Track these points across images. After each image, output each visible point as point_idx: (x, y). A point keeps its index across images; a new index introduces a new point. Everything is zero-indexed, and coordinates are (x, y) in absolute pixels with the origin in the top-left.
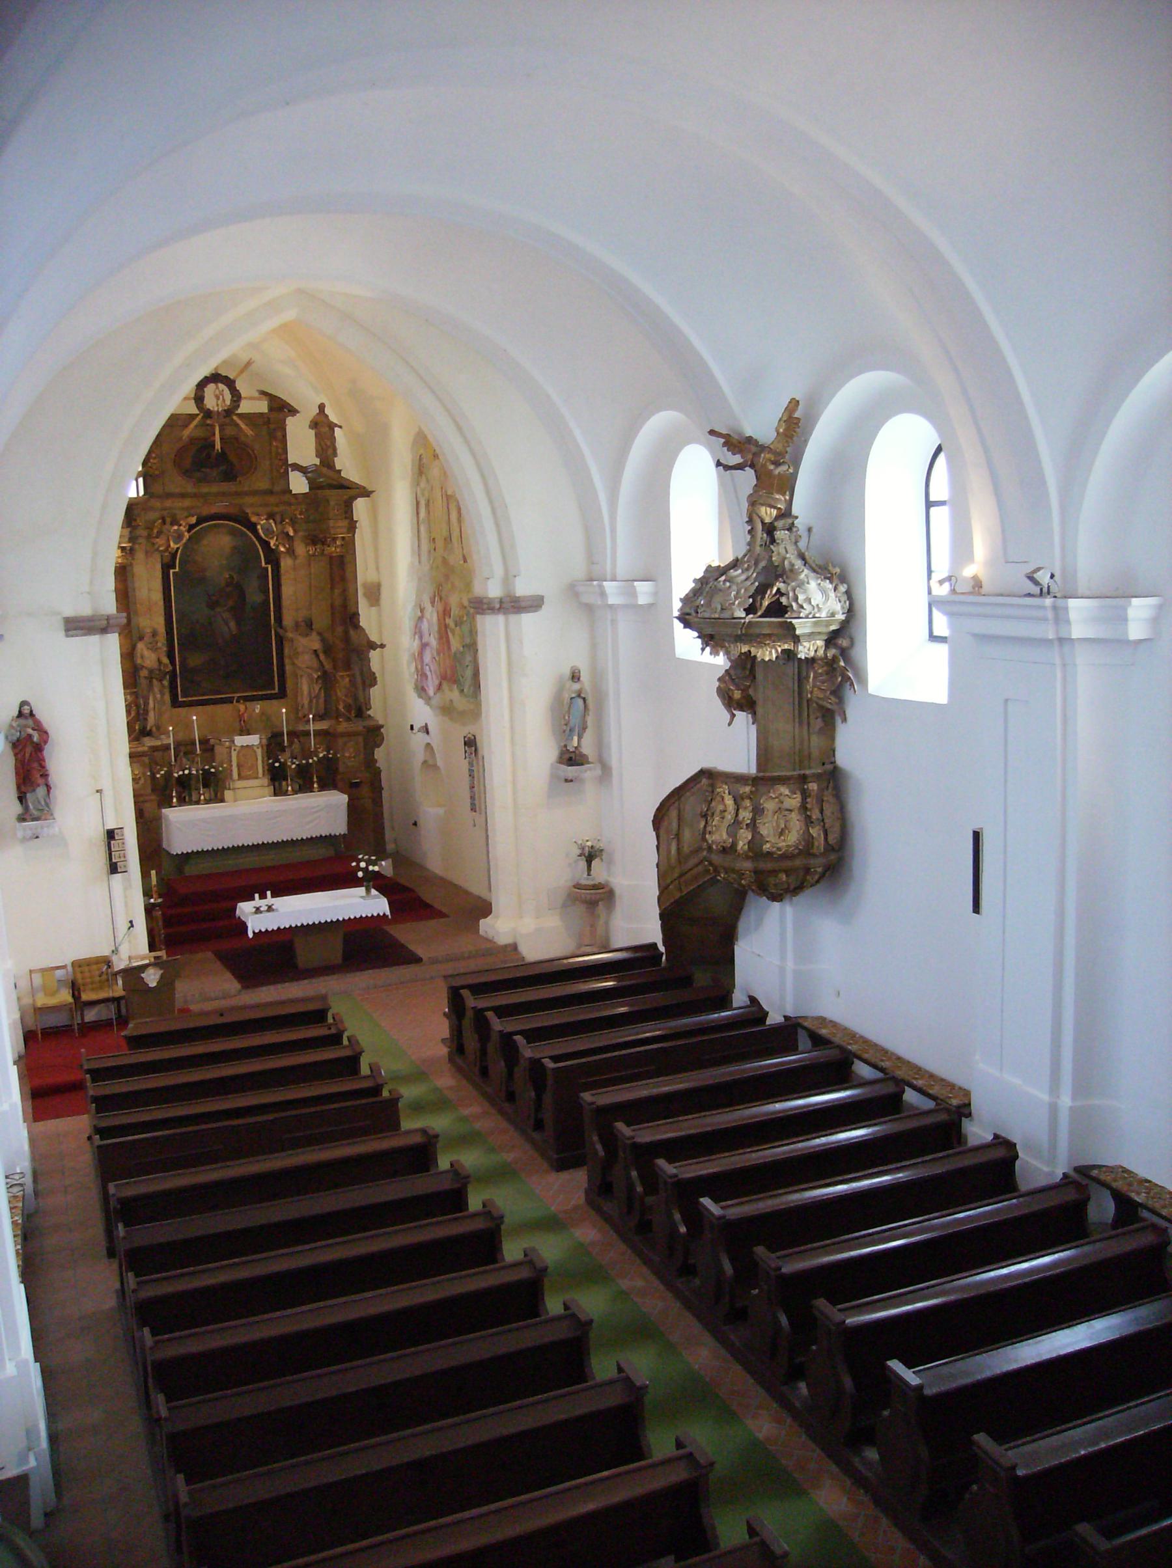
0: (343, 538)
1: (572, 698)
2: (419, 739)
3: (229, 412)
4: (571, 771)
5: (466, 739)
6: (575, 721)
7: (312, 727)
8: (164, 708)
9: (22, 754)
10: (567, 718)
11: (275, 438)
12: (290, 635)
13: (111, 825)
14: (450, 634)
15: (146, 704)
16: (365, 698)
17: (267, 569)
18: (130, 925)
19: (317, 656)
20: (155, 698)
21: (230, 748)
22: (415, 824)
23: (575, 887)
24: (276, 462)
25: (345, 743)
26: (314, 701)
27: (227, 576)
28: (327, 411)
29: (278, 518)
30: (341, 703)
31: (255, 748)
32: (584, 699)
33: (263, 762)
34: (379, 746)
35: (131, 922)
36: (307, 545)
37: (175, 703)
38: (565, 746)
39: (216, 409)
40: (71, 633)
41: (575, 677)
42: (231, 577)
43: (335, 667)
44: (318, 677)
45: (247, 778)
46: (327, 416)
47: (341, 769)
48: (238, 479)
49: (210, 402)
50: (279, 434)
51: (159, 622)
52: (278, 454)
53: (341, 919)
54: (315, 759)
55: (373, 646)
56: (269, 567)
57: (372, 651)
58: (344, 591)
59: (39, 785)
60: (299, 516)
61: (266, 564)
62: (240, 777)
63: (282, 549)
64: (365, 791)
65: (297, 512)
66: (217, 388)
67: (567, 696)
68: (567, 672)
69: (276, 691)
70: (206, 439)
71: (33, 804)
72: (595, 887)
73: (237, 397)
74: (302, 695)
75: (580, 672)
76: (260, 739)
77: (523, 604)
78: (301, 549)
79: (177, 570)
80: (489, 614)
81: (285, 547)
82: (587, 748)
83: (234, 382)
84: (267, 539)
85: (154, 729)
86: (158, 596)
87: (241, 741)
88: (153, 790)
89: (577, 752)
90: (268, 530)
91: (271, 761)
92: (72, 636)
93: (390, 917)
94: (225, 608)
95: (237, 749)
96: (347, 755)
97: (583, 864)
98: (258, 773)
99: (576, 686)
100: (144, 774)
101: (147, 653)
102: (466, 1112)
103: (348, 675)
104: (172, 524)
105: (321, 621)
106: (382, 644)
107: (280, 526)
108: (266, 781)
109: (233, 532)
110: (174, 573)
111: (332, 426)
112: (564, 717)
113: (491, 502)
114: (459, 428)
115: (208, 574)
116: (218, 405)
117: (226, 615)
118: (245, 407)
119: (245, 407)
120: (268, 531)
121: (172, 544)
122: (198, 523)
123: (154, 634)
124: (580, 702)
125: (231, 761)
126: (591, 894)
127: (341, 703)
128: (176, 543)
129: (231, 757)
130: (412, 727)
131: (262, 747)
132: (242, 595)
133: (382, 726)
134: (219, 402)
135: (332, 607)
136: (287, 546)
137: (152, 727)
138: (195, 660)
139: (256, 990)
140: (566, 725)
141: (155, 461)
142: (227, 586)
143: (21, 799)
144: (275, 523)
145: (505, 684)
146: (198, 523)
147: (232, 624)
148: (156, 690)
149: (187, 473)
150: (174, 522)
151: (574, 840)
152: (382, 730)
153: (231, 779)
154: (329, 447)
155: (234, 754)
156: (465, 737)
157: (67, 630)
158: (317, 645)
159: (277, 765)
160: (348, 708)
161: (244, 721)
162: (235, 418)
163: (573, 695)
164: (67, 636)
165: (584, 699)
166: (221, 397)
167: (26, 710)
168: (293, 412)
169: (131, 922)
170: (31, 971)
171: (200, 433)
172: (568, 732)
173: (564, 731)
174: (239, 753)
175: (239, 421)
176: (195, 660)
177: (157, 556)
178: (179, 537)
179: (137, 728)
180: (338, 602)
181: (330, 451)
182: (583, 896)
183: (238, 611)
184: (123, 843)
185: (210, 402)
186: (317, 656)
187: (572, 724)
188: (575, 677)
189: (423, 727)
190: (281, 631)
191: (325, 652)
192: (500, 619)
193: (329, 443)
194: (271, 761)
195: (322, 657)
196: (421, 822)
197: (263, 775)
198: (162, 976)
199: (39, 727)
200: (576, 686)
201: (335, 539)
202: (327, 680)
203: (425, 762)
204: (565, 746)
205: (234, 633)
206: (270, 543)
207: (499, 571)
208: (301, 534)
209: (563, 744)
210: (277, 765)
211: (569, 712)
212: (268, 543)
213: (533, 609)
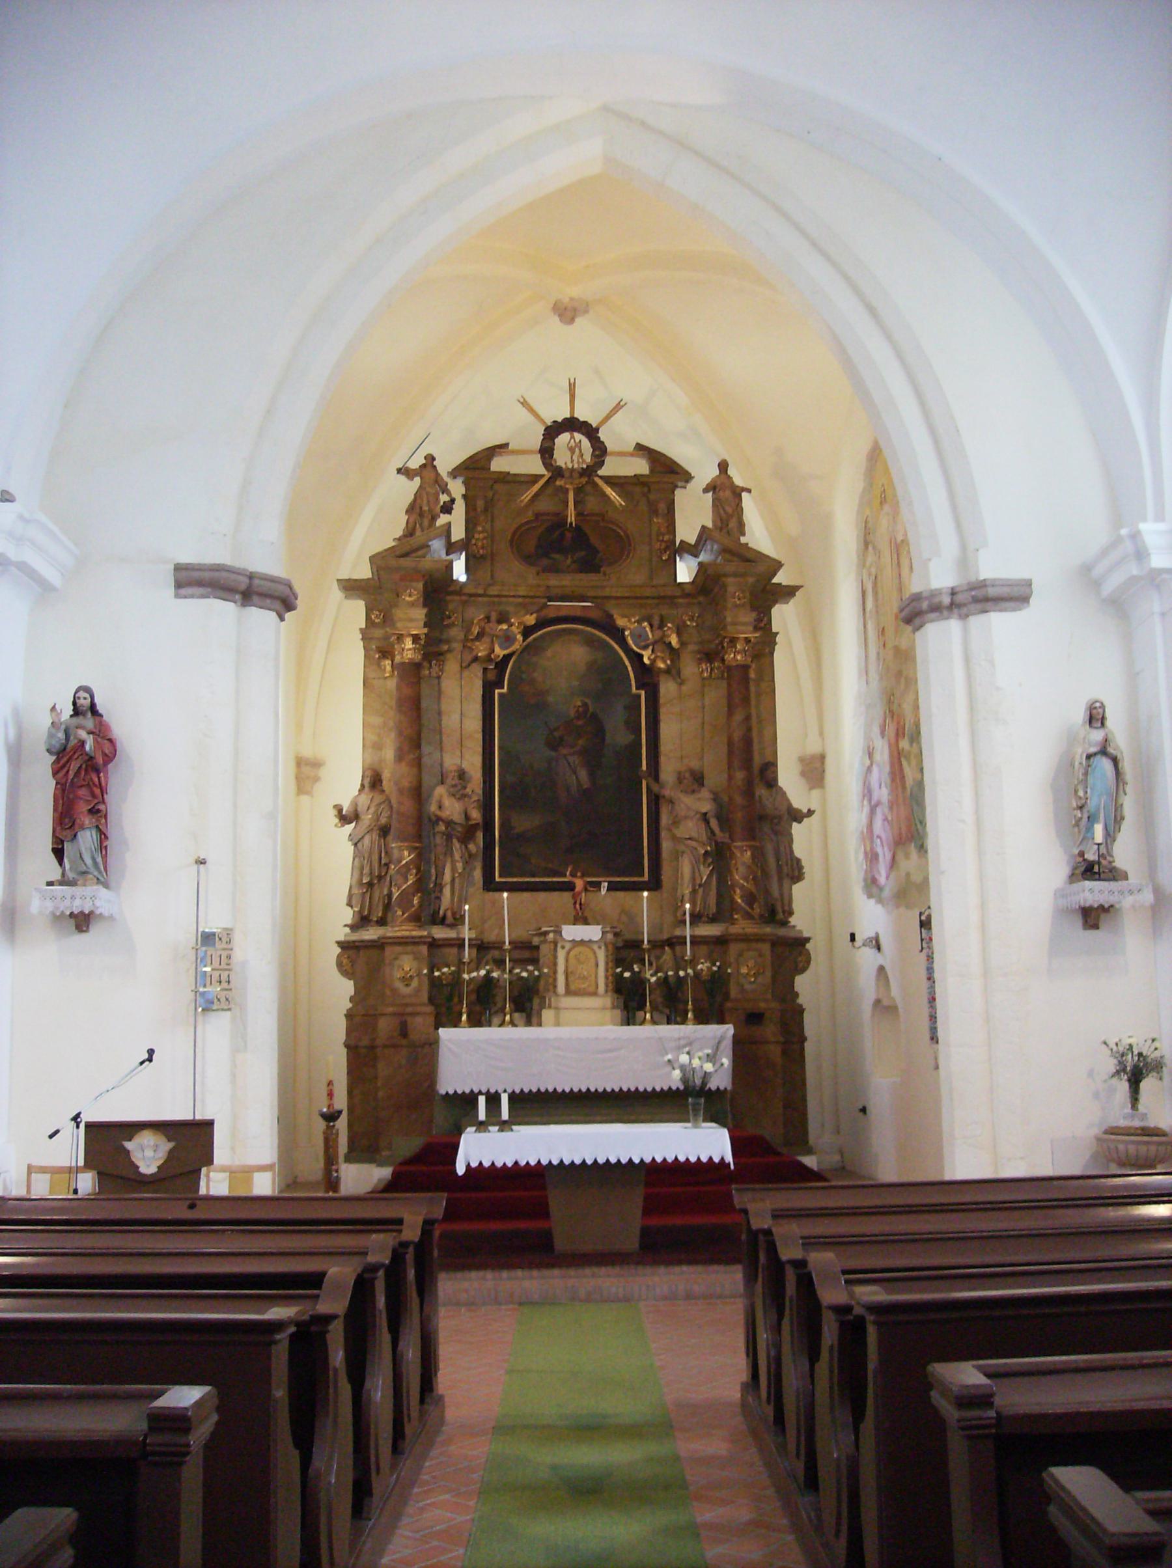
0: (748, 641)
1: (1089, 757)
2: (867, 959)
3: (589, 472)
4: (1092, 892)
5: (923, 918)
6: (1097, 800)
7: (688, 932)
8: (471, 890)
9: (66, 769)
10: (1081, 793)
11: (655, 512)
12: (667, 792)
13: (213, 925)
14: (904, 763)
15: (440, 874)
16: (782, 895)
17: (639, 696)
18: (146, 1056)
19: (707, 822)
20: (454, 870)
21: (555, 943)
22: (864, 1110)
23: (1106, 1132)
24: (657, 545)
25: (740, 955)
26: (701, 891)
27: (579, 703)
28: (731, 472)
29: (656, 622)
30: (738, 891)
31: (595, 947)
32: (1115, 761)
33: (607, 970)
34: (803, 970)
35: (151, 1052)
36: (700, 661)
37: (490, 885)
38: (1082, 854)
39: (570, 466)
40: (183, 591)
41: (1096, 717)
42: (585, 705)
43: (732, 838)
44: (706, 852)
45: (576, 993)
46: (729, 478)
47: (734, 992)
48: (602, 569)
49: (562, 457)
50: (662, 507)
51: (473, 763)
52: (659, 534)
53: (637, 1161)
54: (690, 971)
55: (797, 816)
56: (643, 693)
57: (795, 824)
58: (748, 718)
59: (82, 828)
60: (689, 623)
61: (637, 688)
62: (569, 992)
63: (662, 666)
64: (770, 1030)
65: (685, 618)
66: (572, 437)
67: (1080, 750)
68: (1079, 715)
69: (646, 878)
70: (558, 514)
71: (70, 862)
72: (1146, 1132)
73: (600, 450)
74: (682, 878)
75: (1103, 706)
76: (603, 933)
77: (992, 592)
78: (690, 668)
79: (505, 690)
80: (932, 621)
81: (665, 662)
82: (1124, 854)
83: (597, 430)
84: (638, 651)
85: (449, 914)
86: (474, 724)
87: (572, 932)
88: (431, 1000)
89: (1104, 862)
90: (640, 636)
91: (619, 970)
92: (186, 597)
93: (732, 1167)
94: (572, 751)
95: (568, 946)
96: (744, 970)
97: (1123, 1086)
98: (597, 987)
99: (1097, 736)
100: (419, 974)
101: (447, 802)
102: (707, 1515)
103: (750, 847)
104: (499, 622)
105: (715, 778)
106: (809, 810)
107: (658, 633)
108: (608, 1001)
109: (590, 642)
110: (500, 695)
111: (737, 492)
112: (1076, 791)
113: (932, 430)
114: (872, 311)
115: (551, 699)
116: (572, 461)
117: (575, 760)
118: (610, 468)
119: (610, 468)
120: (639, 636)
121: (497, 649)
122: (539, 625)
123: (462, 775)
124: (1106, 764)
125: (555, 964)
126: (1147, 1143)
127: (738, 891)
128: (502, 648)
129: (555, 957)
130: (853, 937)
131: (606, 945)
132: (599, 732)
133: (808, 940)
134: (575, 458)
135: (730, 743)
136: (669, 662)
137: (446, 911)
138: (524, 823)
139: (459, 1275)
140: (1081, 808)
141: (481, 536)
142: (578, 718)
143: (59, 853)
144: (651, 626)
145: (964, 743)
146: (539, 625)
147: (583, 774)
148: (457, 856)
149: (528, 559)
150: (503, 618)
151: (1103, 1039)
152: (808, 946)
153: (555, 992)
154: (731, 516)
155: (561, 955)
156: (921, 914)
157: (179, 585)
158: (707, 807)
159: (627, 975)
160: (750, 899)
161: (581, 904)
162: (597, 480)
163: (1093, 750)
164: (177, 596)
165: (1115, 761)
166: (577, 450)
167: (84, 702)
168: (687, 477)
169: (151, 1052)
170: (30, 1168)
171: (545, 505)
172: (1085, 819)
173: (1077, 824)
174: (568, 953)
175: (609, 491)
176: (524, 823)
177: (477, 670)
178: (508, 639)
179: (415, 902)
180: (737, 735)
181: (733, 524)
182: (1121, 1147)
183: (593, 757)
184: (229, 957)
185: (562, 457)
186: (707, 822)
187: (1092, 804)
188: (1096, 717)
189: (871, 939)
190: (655, 788)
191: (719, 818)
192: (953, 625)
193: (729, 510)
194: (619, 970)
195: (714, 823)
196: (871, 1110)
197: (606, 991)
198: (171, 1152)
199: (102, 732)
200: (1097, 736)
201: (733, 641)
202: (719, 856)
203: (878, 1002)
204: (1082, 854)
205: (585, 787)
206: (641, 656)
207: (949, 546)
208: (691, 648)
209: (1076, 852)
210: (627, 975)
211: (1085, 782)
212: (641, 657)
213: (1012, 604)
